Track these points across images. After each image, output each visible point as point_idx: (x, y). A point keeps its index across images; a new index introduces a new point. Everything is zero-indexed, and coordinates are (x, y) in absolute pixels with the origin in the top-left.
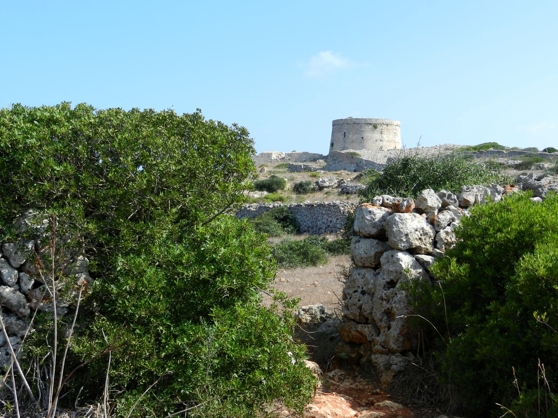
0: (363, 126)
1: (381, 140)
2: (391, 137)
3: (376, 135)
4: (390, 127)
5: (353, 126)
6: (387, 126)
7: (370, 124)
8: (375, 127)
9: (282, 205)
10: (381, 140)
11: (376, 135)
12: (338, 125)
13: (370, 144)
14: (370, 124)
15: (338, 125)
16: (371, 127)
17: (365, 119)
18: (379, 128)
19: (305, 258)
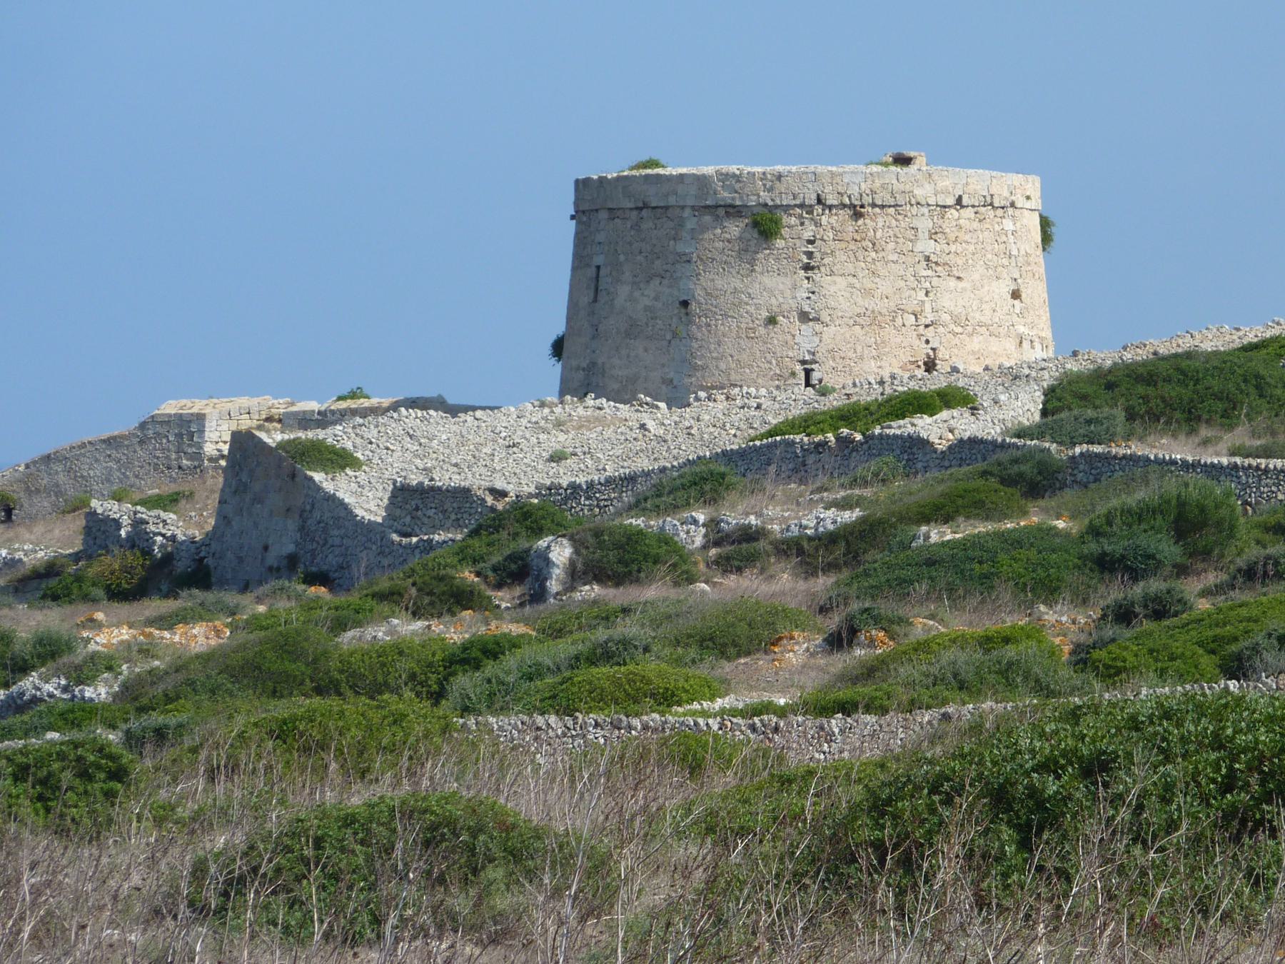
0: (691, 224)
1: (804, 317)
2: (884, 287)
3: (768, 281)
4: (876, 224)
5: (636, 227)
6: (857, 215)
7: (733, 211)
8: (765, 226)
9: (1129, 500)
10: (804, 317)
11: (773, 284)
12: (597, 205)
13: (729, 346)
14: (733, 211)
15: (597, 205)
16: (734, 228)
17: (702, 181)
18: (794, 231)
19: (1135, 840)
